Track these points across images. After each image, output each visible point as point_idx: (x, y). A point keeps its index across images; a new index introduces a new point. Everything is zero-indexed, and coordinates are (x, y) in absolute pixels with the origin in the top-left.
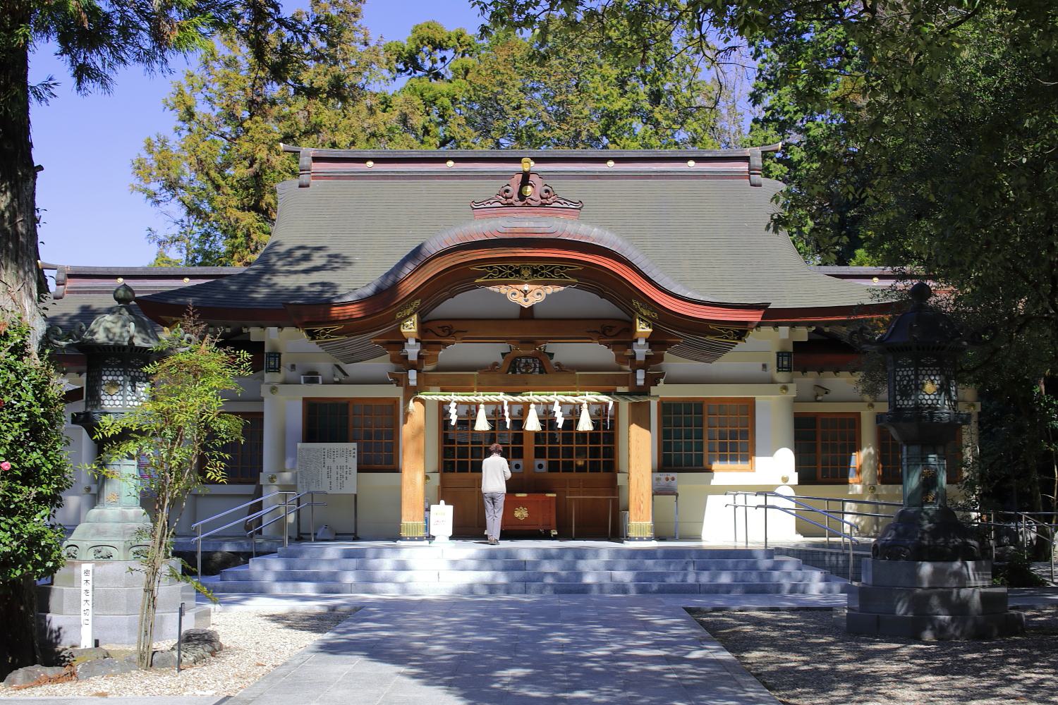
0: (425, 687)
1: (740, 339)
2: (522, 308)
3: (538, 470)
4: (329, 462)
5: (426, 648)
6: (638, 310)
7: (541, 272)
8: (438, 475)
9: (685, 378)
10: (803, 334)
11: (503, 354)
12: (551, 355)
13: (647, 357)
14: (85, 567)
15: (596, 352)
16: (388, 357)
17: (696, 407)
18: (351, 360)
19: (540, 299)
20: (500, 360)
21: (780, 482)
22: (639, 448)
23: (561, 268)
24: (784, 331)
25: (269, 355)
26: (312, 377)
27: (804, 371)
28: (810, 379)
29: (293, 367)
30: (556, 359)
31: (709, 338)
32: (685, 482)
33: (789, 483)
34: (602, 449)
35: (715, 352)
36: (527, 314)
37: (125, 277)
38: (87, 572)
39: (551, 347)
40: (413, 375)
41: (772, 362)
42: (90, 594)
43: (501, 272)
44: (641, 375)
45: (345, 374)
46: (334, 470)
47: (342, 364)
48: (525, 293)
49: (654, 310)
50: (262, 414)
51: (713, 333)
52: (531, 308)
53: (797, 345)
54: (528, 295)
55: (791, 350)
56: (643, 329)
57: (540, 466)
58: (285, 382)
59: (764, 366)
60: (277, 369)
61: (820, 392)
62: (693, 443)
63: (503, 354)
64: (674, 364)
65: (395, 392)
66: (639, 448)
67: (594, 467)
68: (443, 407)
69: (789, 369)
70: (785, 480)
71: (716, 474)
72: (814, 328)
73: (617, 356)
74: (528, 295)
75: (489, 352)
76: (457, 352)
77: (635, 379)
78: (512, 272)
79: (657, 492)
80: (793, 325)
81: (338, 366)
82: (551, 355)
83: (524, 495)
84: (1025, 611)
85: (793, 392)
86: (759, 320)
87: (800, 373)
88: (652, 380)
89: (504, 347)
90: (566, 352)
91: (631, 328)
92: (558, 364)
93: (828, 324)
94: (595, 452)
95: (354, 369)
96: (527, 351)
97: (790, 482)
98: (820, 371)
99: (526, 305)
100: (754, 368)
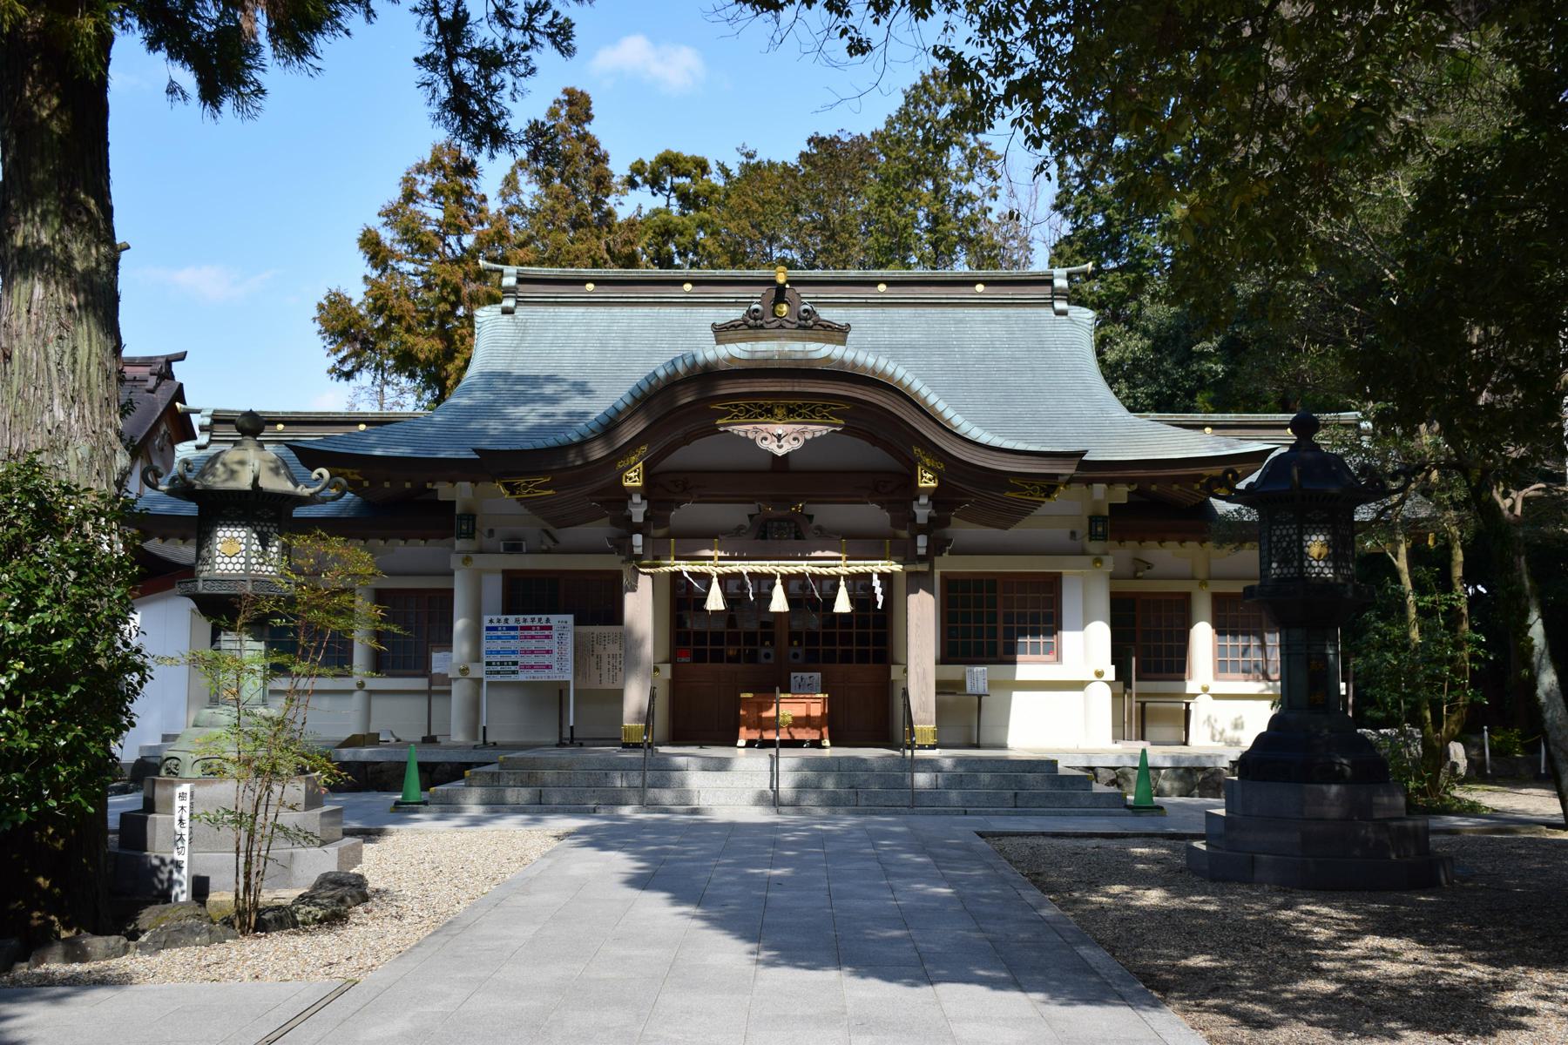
1: (1048, 496)
2: (774, 456)
3: (771, 661)
4: (598, 649)
6: (920, 460)
7: (797, 408)
8: (668, 666)
9: (980, 551)
10: (1122, 494)
11: (751, 516)
12: (811, 517)
13: (930, 519)
14: (185, 788)
15: (871, 515)
16: (607, 519)
17: (988, 583)
18: (562, 522)
19: (797, 445)
20: (747, 523)
21: (1093, 678)
23: (824, 407)
24: (1099, 489)
25: (461, 517)
26: (513, 547)
27: (1121, 541)
28: (1128, 550)
29: (491, 532)
30: (816, 521)
31: (1008, 494)
32: (978, 676)
33: (1105, 678)
34: (875, 632)
35: (1010, 515)
36: (780, 464)
37: (286, 423)
38: (182, 796)
39: (812, 509)
40: (638, 539)
41: (1083, 528)
42: (187, 823)
43: (748, 411)
44: (922, 541)
45: (556, 541)
46: (605, 659)
47: (550, 528)
48: (779, 438)
49: (940, 460)
50: (452, 591)
51: (1015, 489)
52: (786, 456)
53: (1114, 508)
54: (780, 438)
55: (1106, 512)
56: (927, 481)
57: (796, 656)
58: (480, 552)
59: (1073, 534)
60: (470, 535)
61: (1140, 568)
62: (994, 624)
63: (751, 516)
64: (963, 531)
66: (921, 616)
67: (863, 658)
69: (1104, 537)
70: (1099, 674)
71: (1019, 667)
72: (1135, 487)
73: (893, 519)
74: (780, 438)
75: (735, 514)
76: (688, 513)
77: (915, 547)
78: (763, 408)
79: (943, 687)
80: (1111, 482)
81: (547, 532)
82: (811, 517)
83: (750, 695)
85: (1109, 565)
86: (1072, 471)
87: (1116, 543)
89: (752, 509)
92: (819, 528)
93: (1154, 480)
94: (863, 639)
95: (570, 535)
96: (780, 505)
97: (1105, 678)
98: (1141, 541)
99: (780, 452)
100: (1060, 534)
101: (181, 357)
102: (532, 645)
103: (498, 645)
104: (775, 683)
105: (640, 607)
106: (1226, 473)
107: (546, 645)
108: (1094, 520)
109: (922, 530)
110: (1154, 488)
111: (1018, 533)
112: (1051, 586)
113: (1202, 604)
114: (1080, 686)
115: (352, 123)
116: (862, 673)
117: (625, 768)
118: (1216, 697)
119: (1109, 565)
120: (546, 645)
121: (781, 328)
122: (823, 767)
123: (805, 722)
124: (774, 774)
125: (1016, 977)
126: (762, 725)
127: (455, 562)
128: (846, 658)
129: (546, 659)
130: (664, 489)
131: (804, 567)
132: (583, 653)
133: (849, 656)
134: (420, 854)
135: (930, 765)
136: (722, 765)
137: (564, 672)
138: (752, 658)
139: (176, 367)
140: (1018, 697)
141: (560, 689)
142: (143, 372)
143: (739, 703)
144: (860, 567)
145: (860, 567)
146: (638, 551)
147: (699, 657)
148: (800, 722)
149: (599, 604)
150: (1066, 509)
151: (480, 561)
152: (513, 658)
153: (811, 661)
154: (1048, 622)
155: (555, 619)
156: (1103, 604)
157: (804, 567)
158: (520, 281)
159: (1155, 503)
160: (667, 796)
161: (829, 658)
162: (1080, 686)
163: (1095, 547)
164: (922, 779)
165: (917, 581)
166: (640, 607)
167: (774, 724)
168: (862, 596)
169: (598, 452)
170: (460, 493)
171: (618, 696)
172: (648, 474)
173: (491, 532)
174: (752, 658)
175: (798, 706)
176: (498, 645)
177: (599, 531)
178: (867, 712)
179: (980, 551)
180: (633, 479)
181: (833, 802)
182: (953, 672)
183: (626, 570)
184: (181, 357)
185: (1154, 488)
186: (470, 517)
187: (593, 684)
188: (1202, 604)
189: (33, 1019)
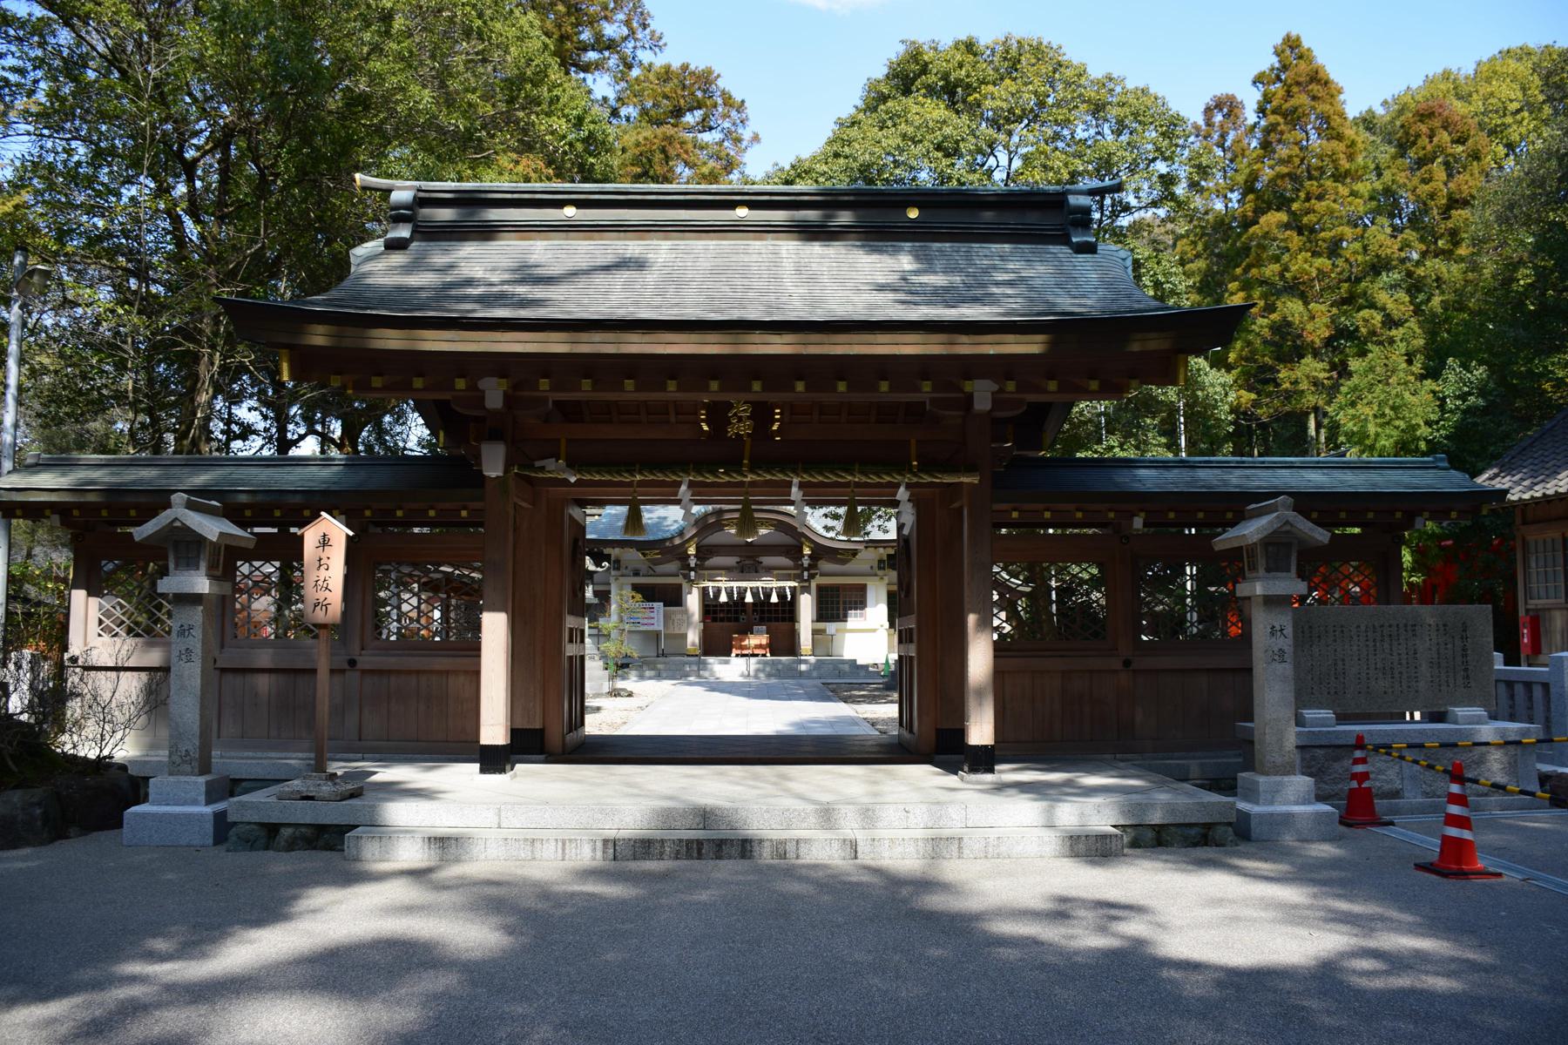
0: (1142, 902)
5: (1093, 849)
9: (831, 573)
22: (806, 606)
26: (636, 574)
32: (831, 627)
34: (787, 610)
35: (844, 562)
39: (762, 559)
56: (807, 551)
62: (835, 605)
65: (679, 580)
66: (806, 606)
67: (784, 620)
68: (705, 590)
75: (731, 561)
79: (815, 632)
84: (140, 524)
85: (886, 580)
88: (812, 576)
90: (768, 560)
91: (801, 550)
94: (784, 612)
100: (865, 567)
104: (747, 631)
105: (693, 601)
108: (880, 561)
112: (862, 589)
113: (750, 611)
114: (874, 631)
116: (783, 626)
117: (690, 664)
119: (886, 580)
122: (766, 663)
123: (760, 646)
124: (748, 665)
125: (811, 699)
126: (742, 648)
127: (612, 580)
128: (777, 620)
130: (704, 552)
131: (759, 584)
132: (667, 617)
133: (779, 616)
134: (630, 683)
135: (806, 662)
136: (727, 662)
137: (659, 626)
138: (737, 620)
140: (848, 636)
141: (657, 634)
143: (732, 639)
144: (781, 584)
145: (781, 584)
147: (715, 620)
148: (757, 647)
149: (673, 598)
153: (761, 621)
154: (861, 604)
155: (655, 605)
156: (884, 597)
157: (759, 584)
160: (706, 674)
161: (770, 620)
162: (874, 631)
163: (880, 573)
164: (803, 667)
165: (806, 590)
166: (693, 601)
167: (746, 648)
168: (782, 595)
169: (677, 541)
171: (684, 636)
172: (697, 549)
174: (737, 620)
175: (757, 639)
177: (673, 566)
178: (785, 644)
179: (831, 573)
180: (692, 551)
181: (769, 676)
182: (821, 625)
183: (685, 586)
187: (670, 631)
188: (750, 611)
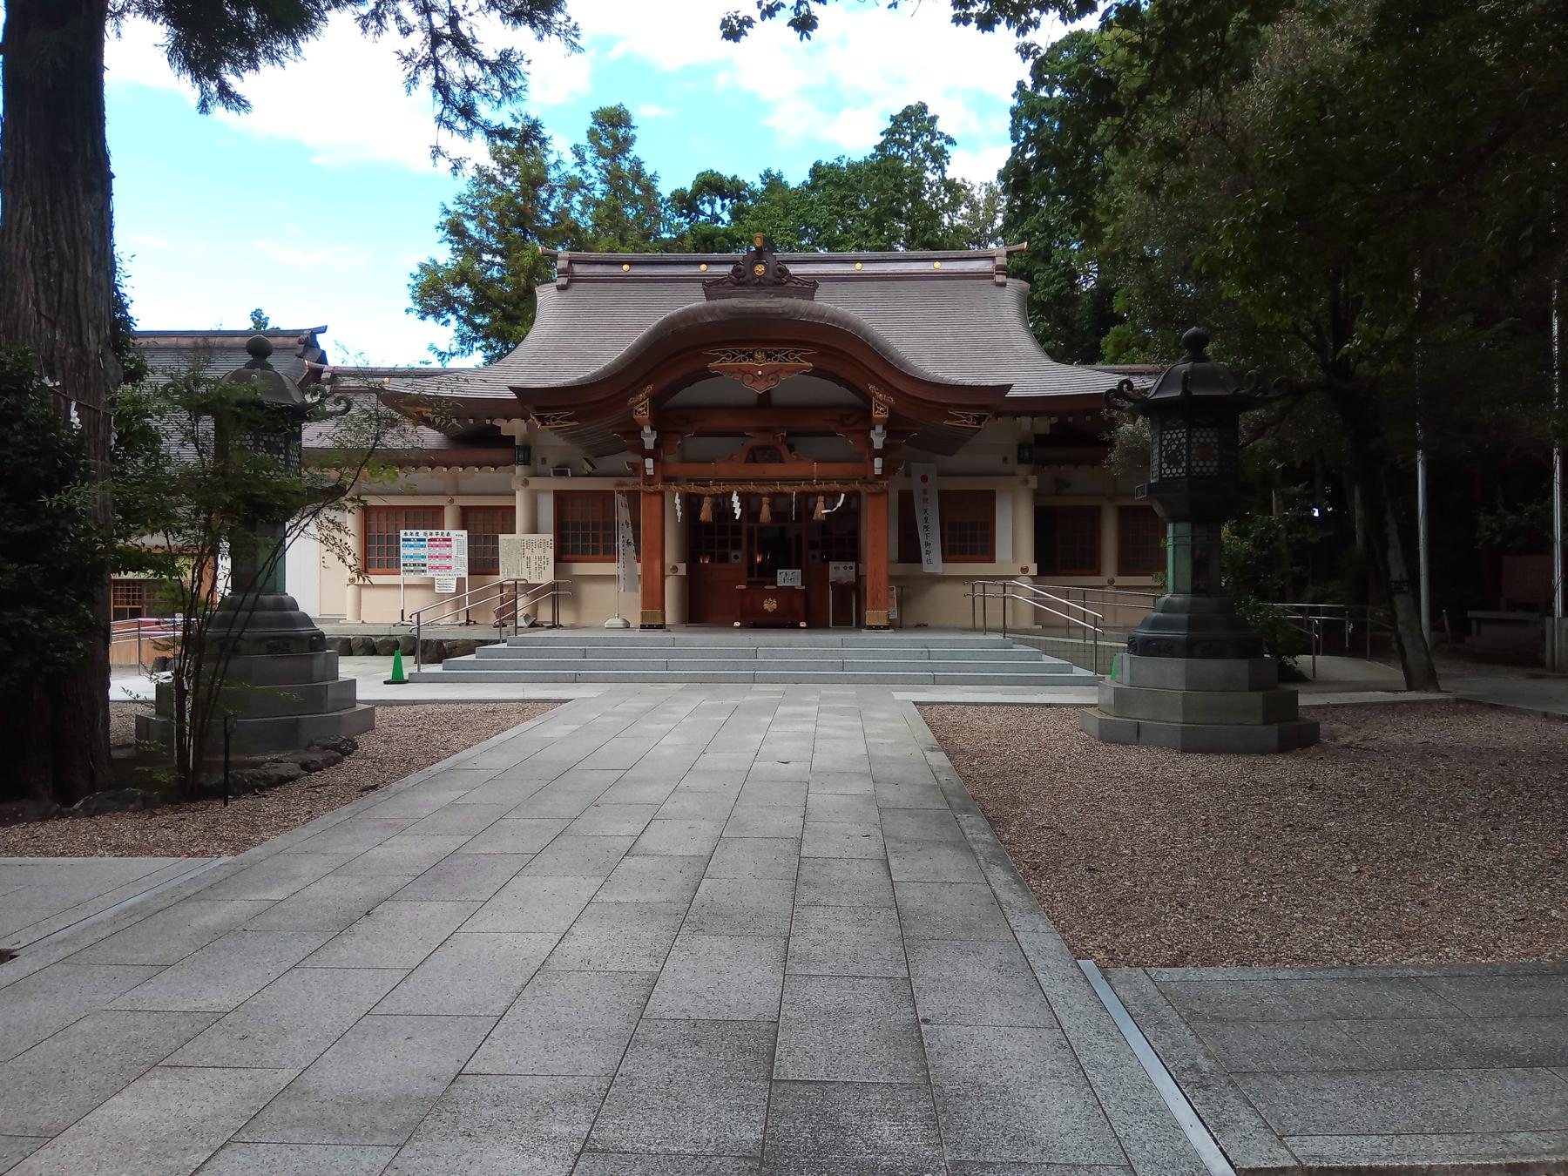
10: (1044, 426)
13: (884, 445)
26: (560, 472)
40: (649, 463)
59: (1005, 459)
70: (1025, 570)
72: (1054, 420)
101: (323, 330)
102: (437, 552)
103: (411, 551)
106: (1122, 383)
107: (446, 551)
108: (1021, 447)
109: (878, 453)
110: (1070, 419)
111: (960, 460)
115: (339, 87)
118: (1118, 588)
120: (446, 551)
121: (760, 284)
127: (515, 484)
129: (447, 562)
139: (320, 338)
142: (293, 341)
146: (650, 472)
150: (1001, 435)
151: (535, 483)
152: (422, 561)
158: (571, 262)
159: (1068, 431)
170: (515, 428)
173: (544, 461)
176: (411, 551)
184: (323, 330)
185: (1070, 419)
186: (526, 449)
189: (554, 729)
